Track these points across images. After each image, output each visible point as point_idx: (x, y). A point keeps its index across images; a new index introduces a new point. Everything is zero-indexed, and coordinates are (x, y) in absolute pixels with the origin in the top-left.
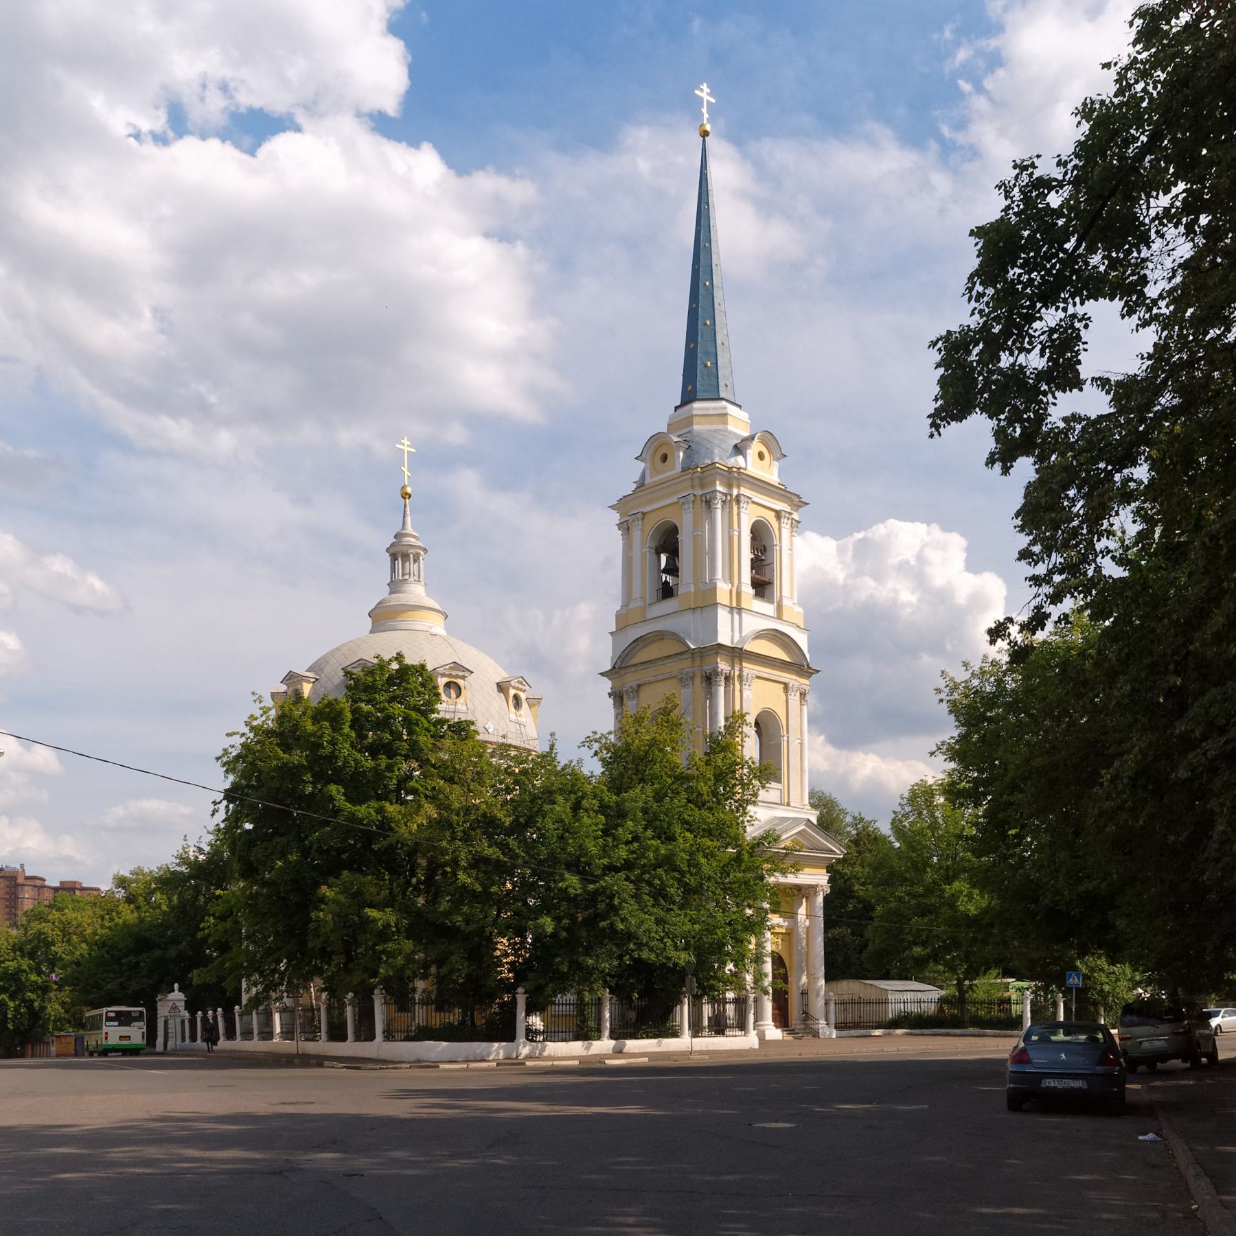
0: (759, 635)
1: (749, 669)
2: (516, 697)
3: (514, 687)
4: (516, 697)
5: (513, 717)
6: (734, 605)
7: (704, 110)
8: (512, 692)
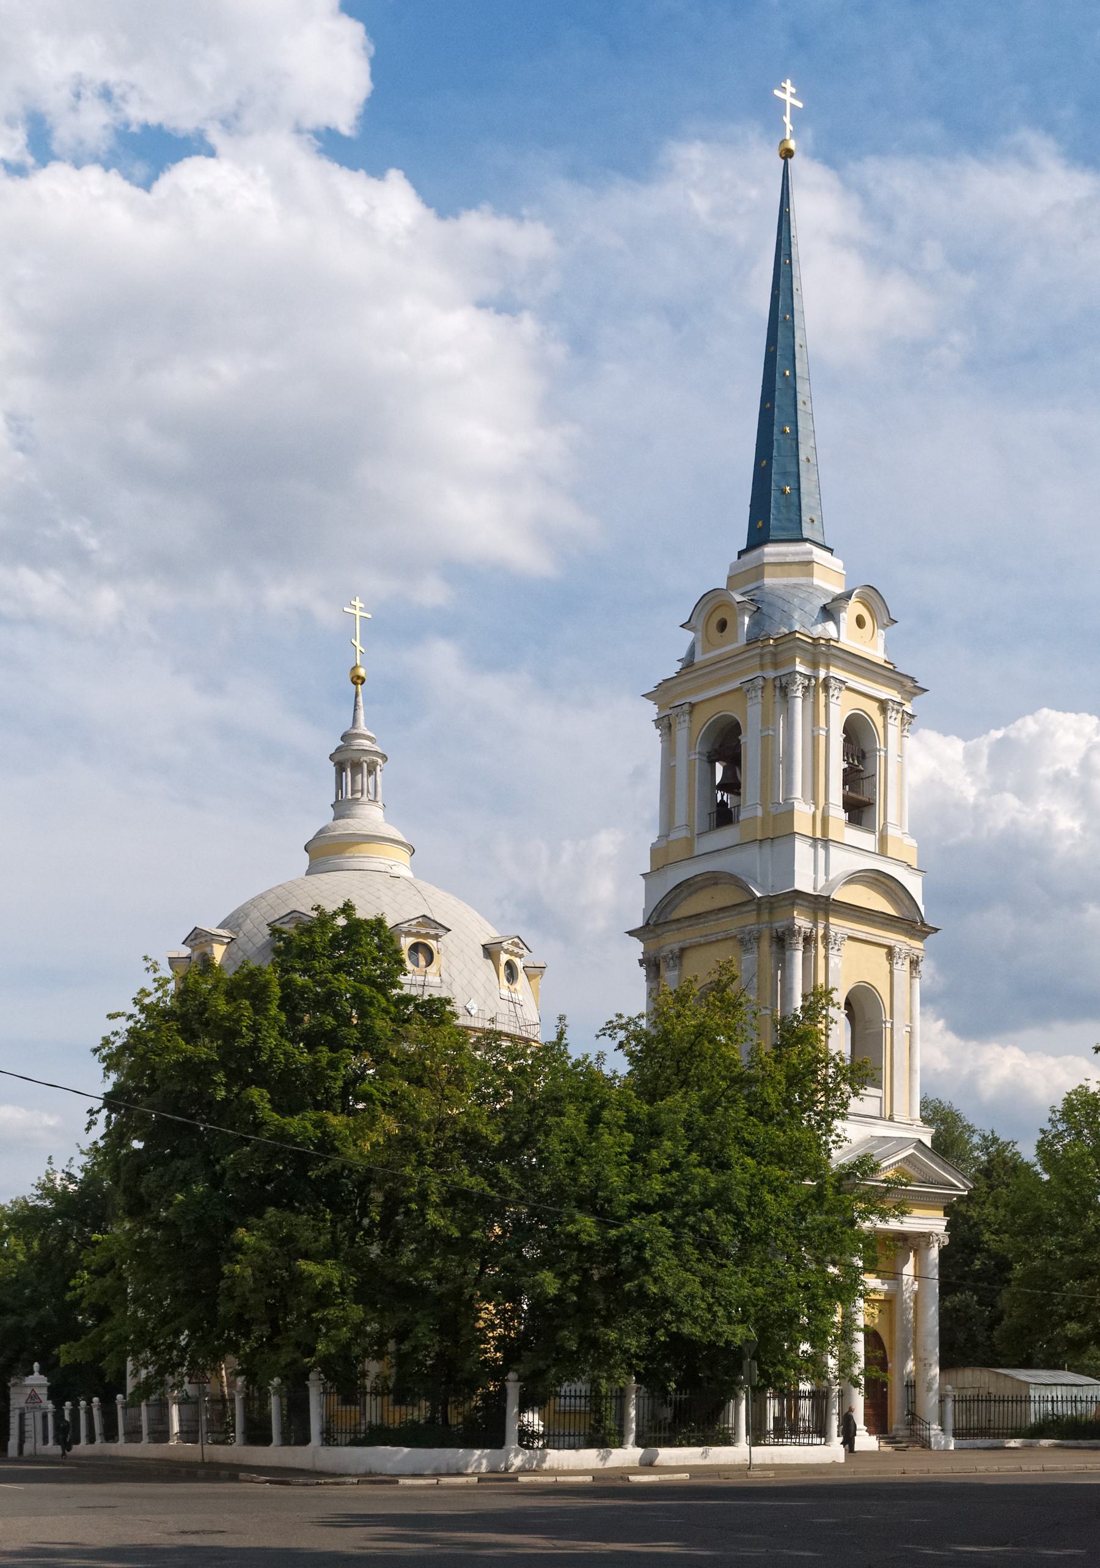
1: (839, 926)
2: (510, 965)
3: (507, 951)
4: (510, 965)
5: (505, 993)
6: (819, 835)
7: (787, 120)
8: (504, 958)
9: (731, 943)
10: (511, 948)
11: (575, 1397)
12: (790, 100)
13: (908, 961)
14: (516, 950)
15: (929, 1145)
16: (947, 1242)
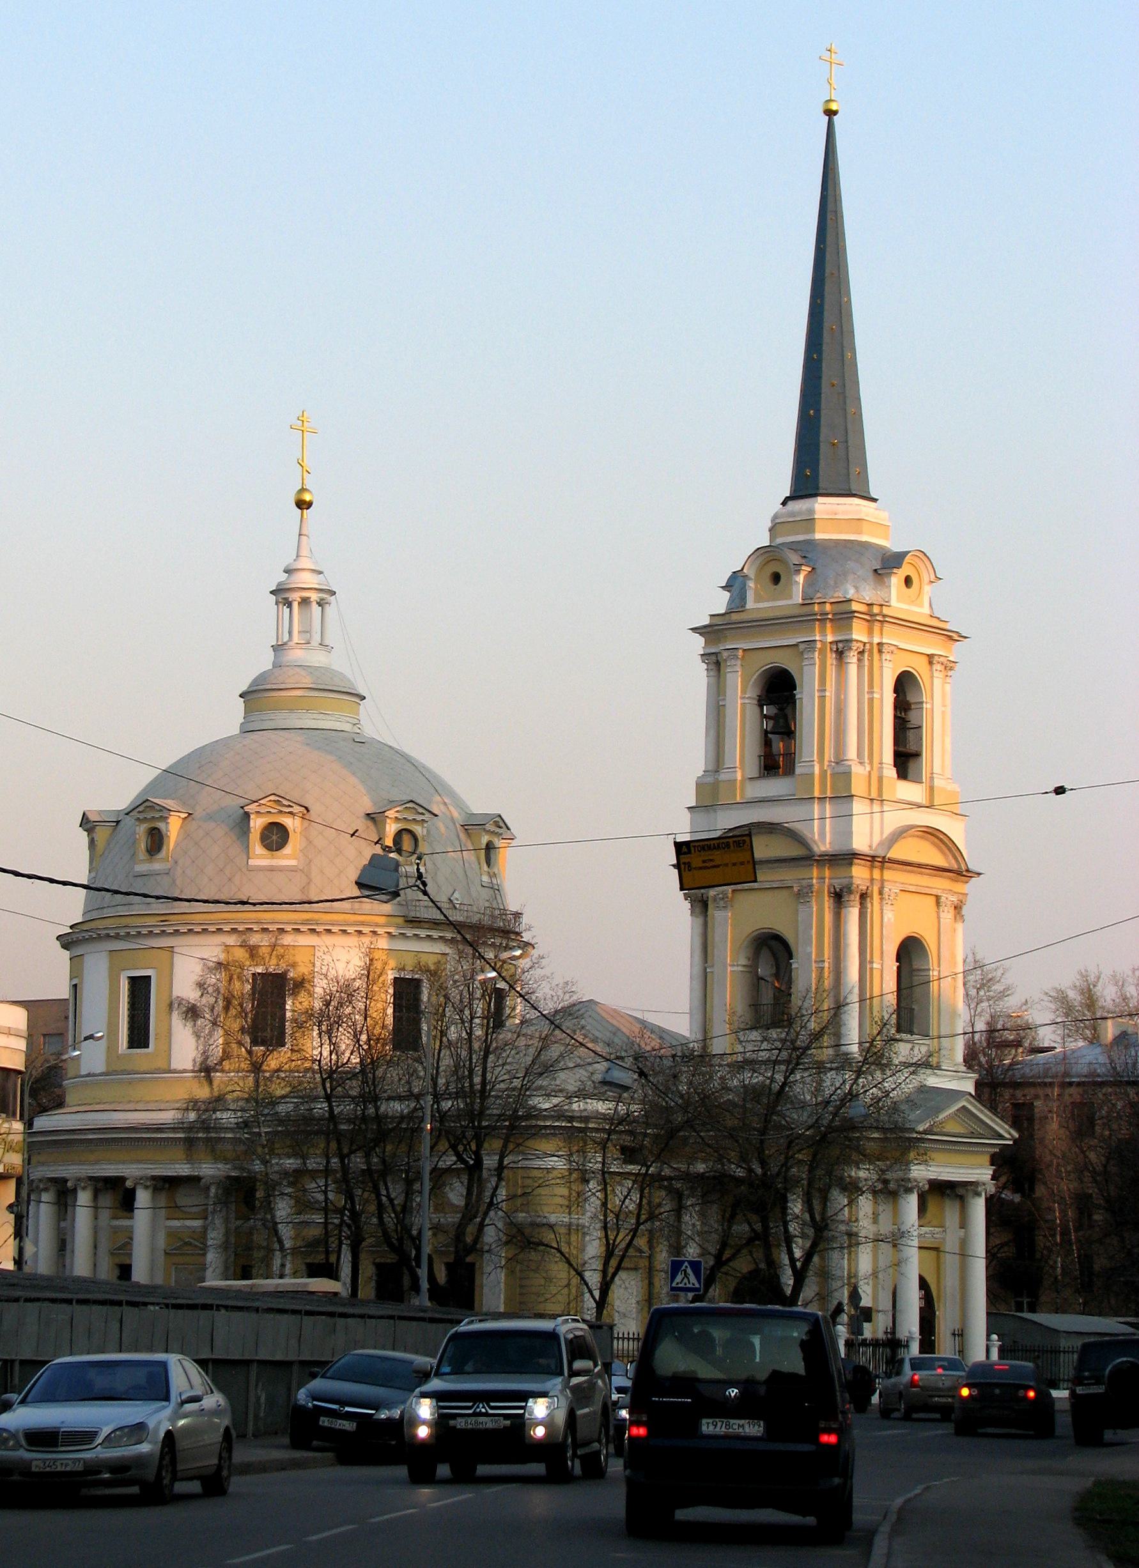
0: (901, 834)
1: (894, 878)
5: (485, 878)
6: (874, 795)
9: (785, 893)
10: (493, 828)
11: (623, 1339)
14: (498, 830)
15: (973, 1093)
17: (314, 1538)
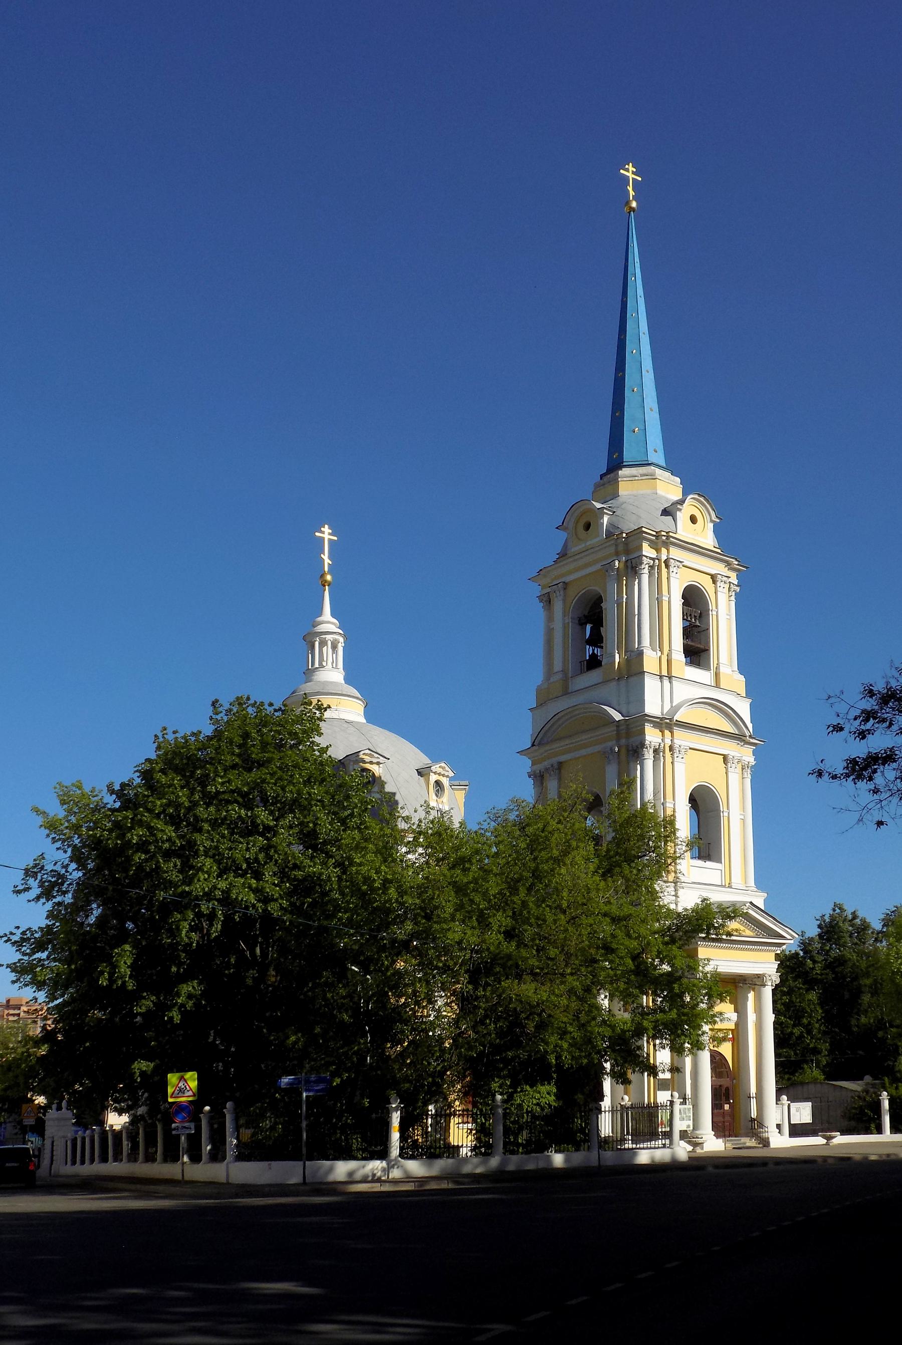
1: (682, 738)
2: (438, 784)
3: (435, 773)
4: (438, 784)
7: (630, 188)
8: (433, 778)
10: (440, 770)
12: (631, 176)
13: (740, 766)
16: (778, 981)
17: (574, 1302)
